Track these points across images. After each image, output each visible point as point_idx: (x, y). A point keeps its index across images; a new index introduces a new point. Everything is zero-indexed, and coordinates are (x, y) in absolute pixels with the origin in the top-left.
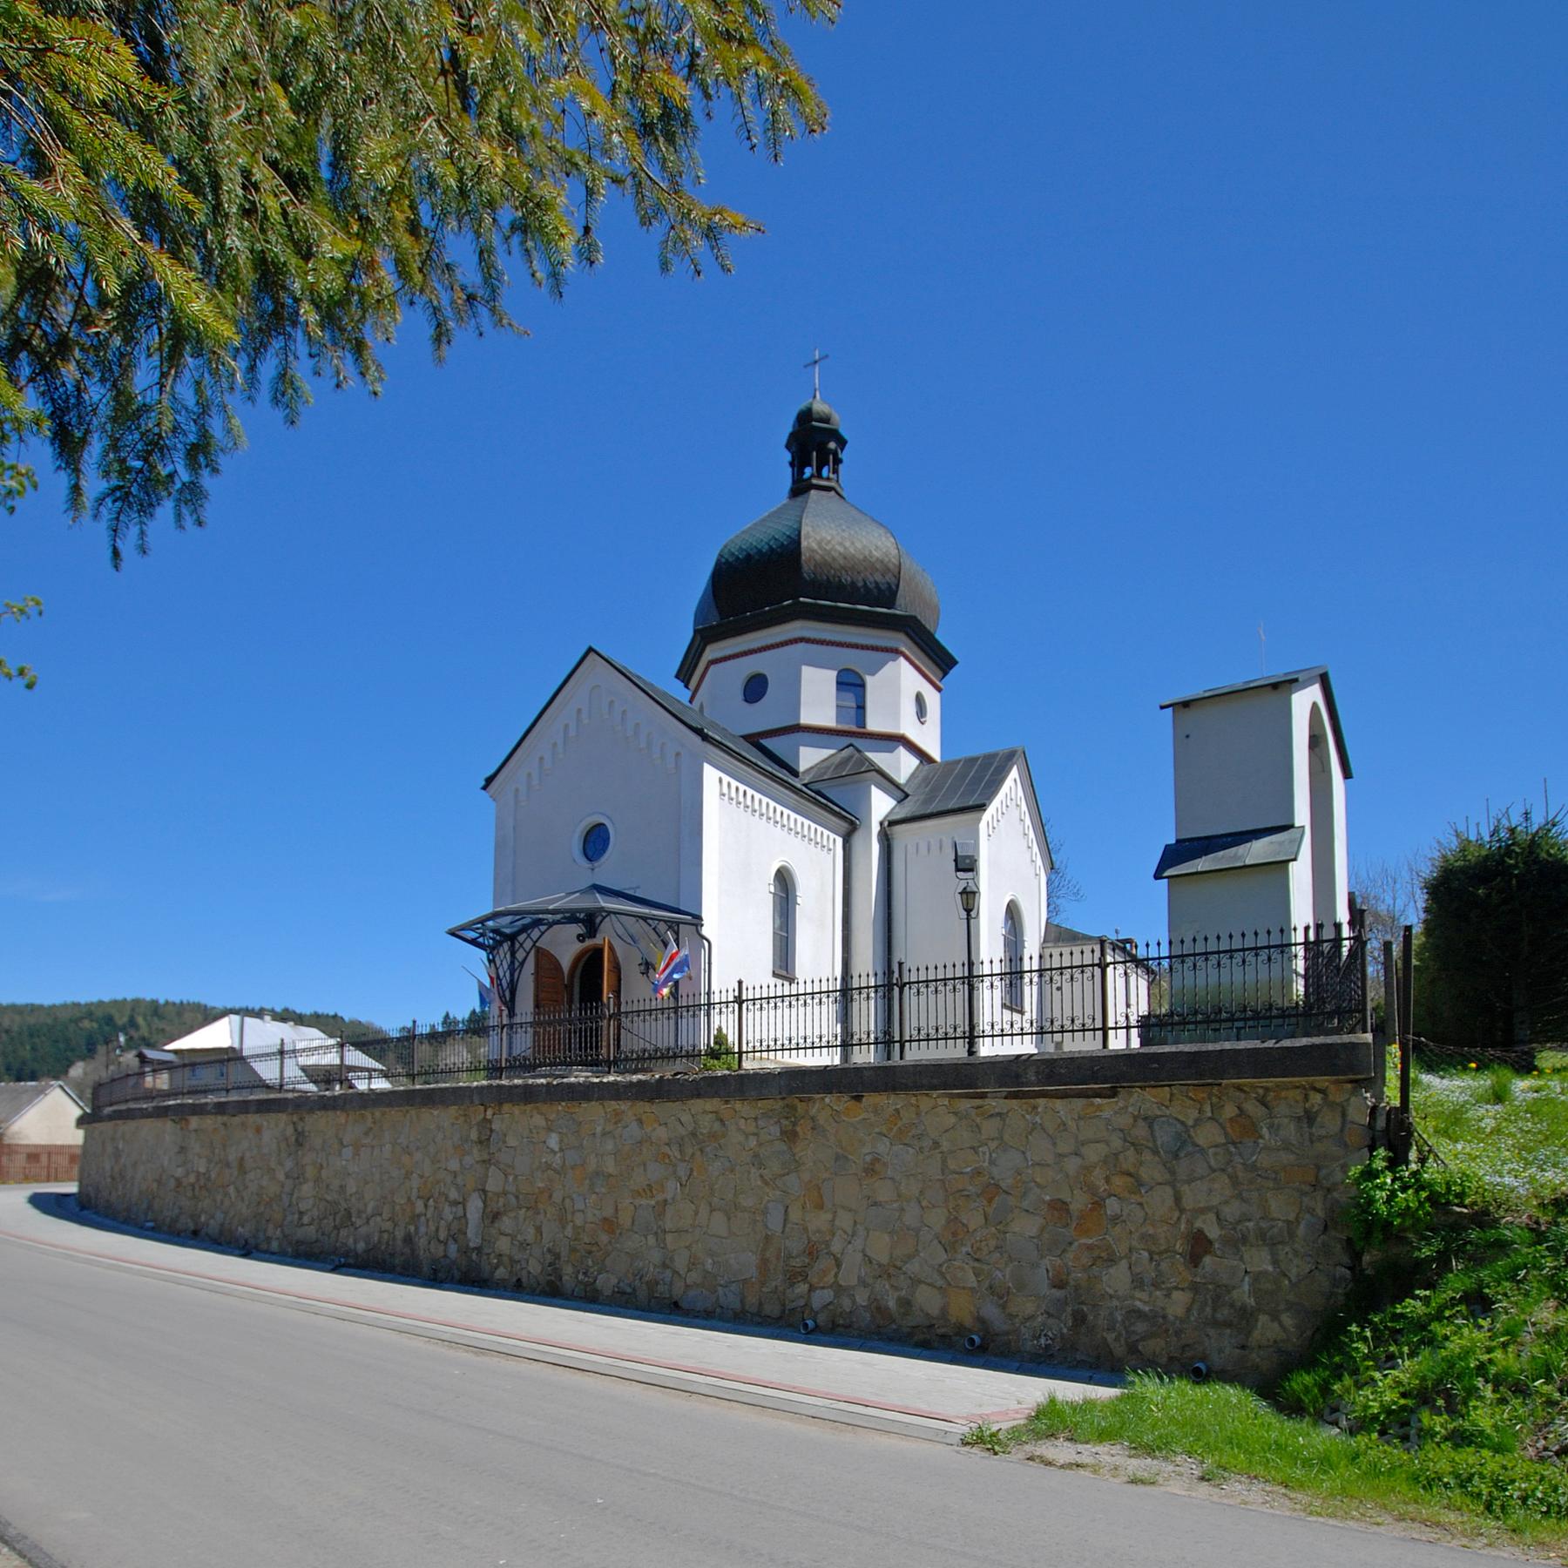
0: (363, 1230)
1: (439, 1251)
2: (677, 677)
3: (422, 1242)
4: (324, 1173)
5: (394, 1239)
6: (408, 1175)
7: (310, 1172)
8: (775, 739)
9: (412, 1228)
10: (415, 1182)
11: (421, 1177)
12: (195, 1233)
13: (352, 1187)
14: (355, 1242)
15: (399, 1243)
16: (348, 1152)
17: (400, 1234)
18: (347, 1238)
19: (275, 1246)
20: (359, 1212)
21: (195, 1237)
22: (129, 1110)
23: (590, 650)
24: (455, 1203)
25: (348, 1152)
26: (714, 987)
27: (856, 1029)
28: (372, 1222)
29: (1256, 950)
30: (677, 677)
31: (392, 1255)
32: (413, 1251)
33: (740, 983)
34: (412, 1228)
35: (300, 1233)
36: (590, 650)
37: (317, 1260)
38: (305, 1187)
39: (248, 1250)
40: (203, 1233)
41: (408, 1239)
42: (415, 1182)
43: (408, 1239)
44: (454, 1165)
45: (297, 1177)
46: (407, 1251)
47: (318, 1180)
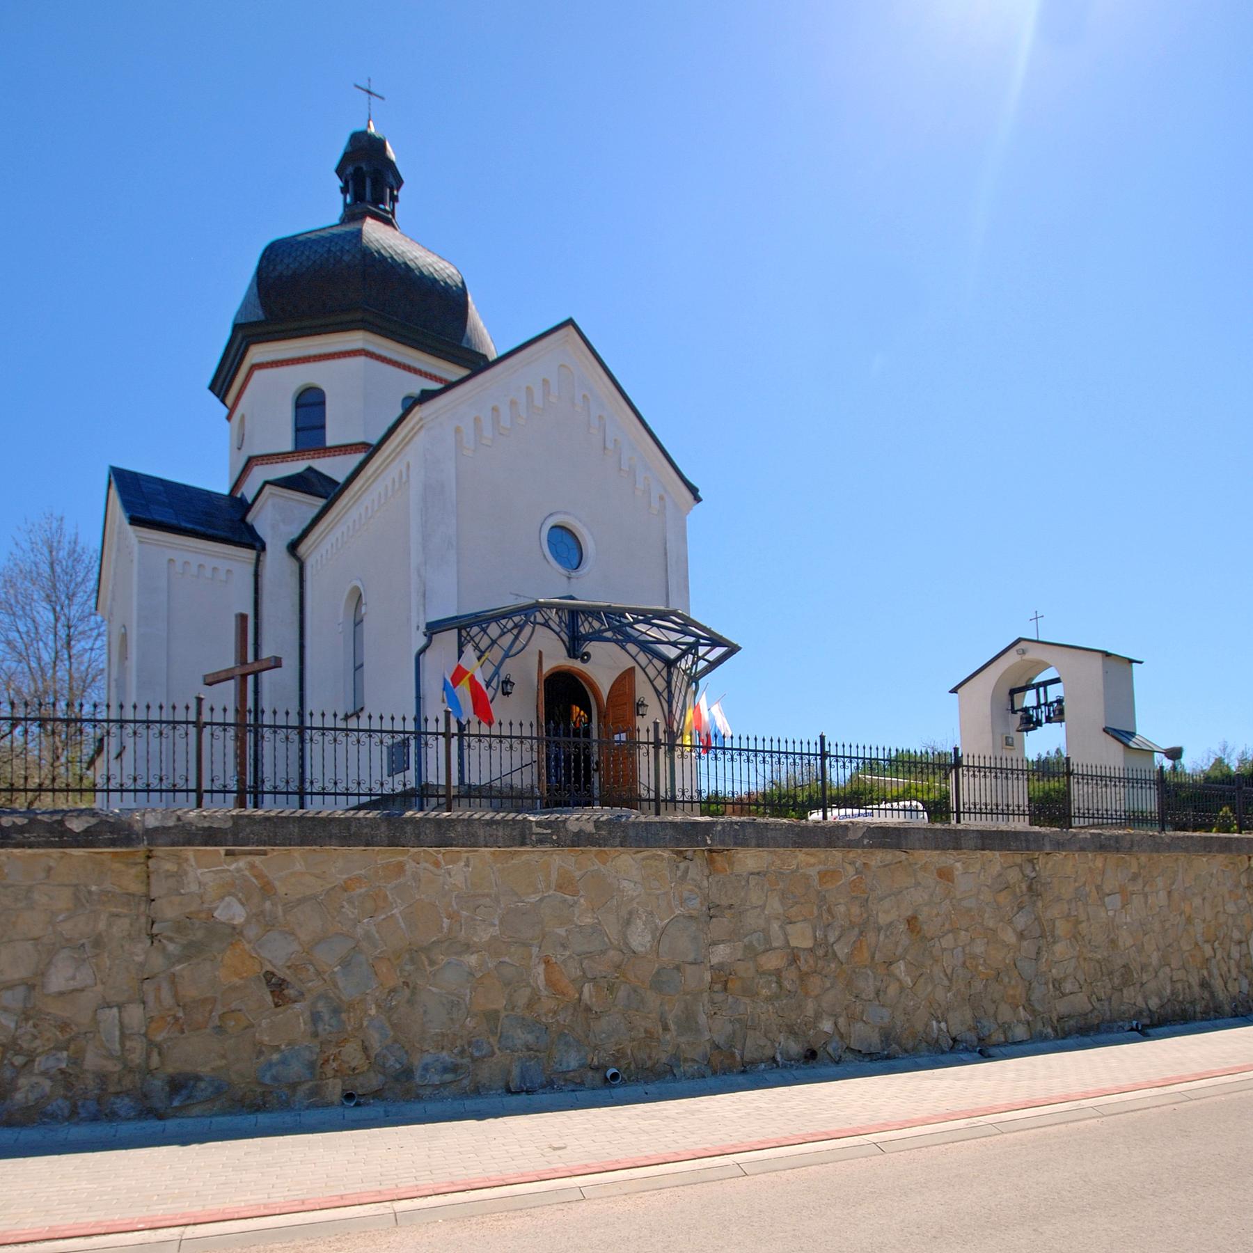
0: (1152, 986)
1: (1234, 988)
2: (212, 388)
3: (1217, 984)
4: (1083, 927)
5: (1190, 987)
6: (1189, 920)
7: (1062, 928)
8: (316, 511)
9: (1206, 973)
10: (1199, 927)
11: (1204, 921)
12: (811, 1055)
13: (1125, 940)
14: (1145, 999)
15: (1196, 989)
16: (1115, 901)
17: (1194, 981)
18: (1133, 998)
19: (1020, 1032)
20: (1144, 968)
21: (813, 1062)
22: (1117, 839)
23: (570, 322)
24: (1240, 943)
25: (1115, 901)
26: (266, 704)
27: (231, 745)
28: (1161, 974)
29: (148, 723)
30: (212, 388)
31: (1193, 1003)
32: (1212, 994)
33: (822, 738)
34: (1206, 973)
35: (1062, 1007)
36: (570, 322)
37: (1109, 1030)
38: (1059, 948)
39: (981, 1048)
40: (820, 1054)
41: (1204, 984)
42: (1199, 927)
43: (1204, 984)
44: (1231, 908)
45: (1043, 934)
46: (1206, 995)
47: (1075, 936)
